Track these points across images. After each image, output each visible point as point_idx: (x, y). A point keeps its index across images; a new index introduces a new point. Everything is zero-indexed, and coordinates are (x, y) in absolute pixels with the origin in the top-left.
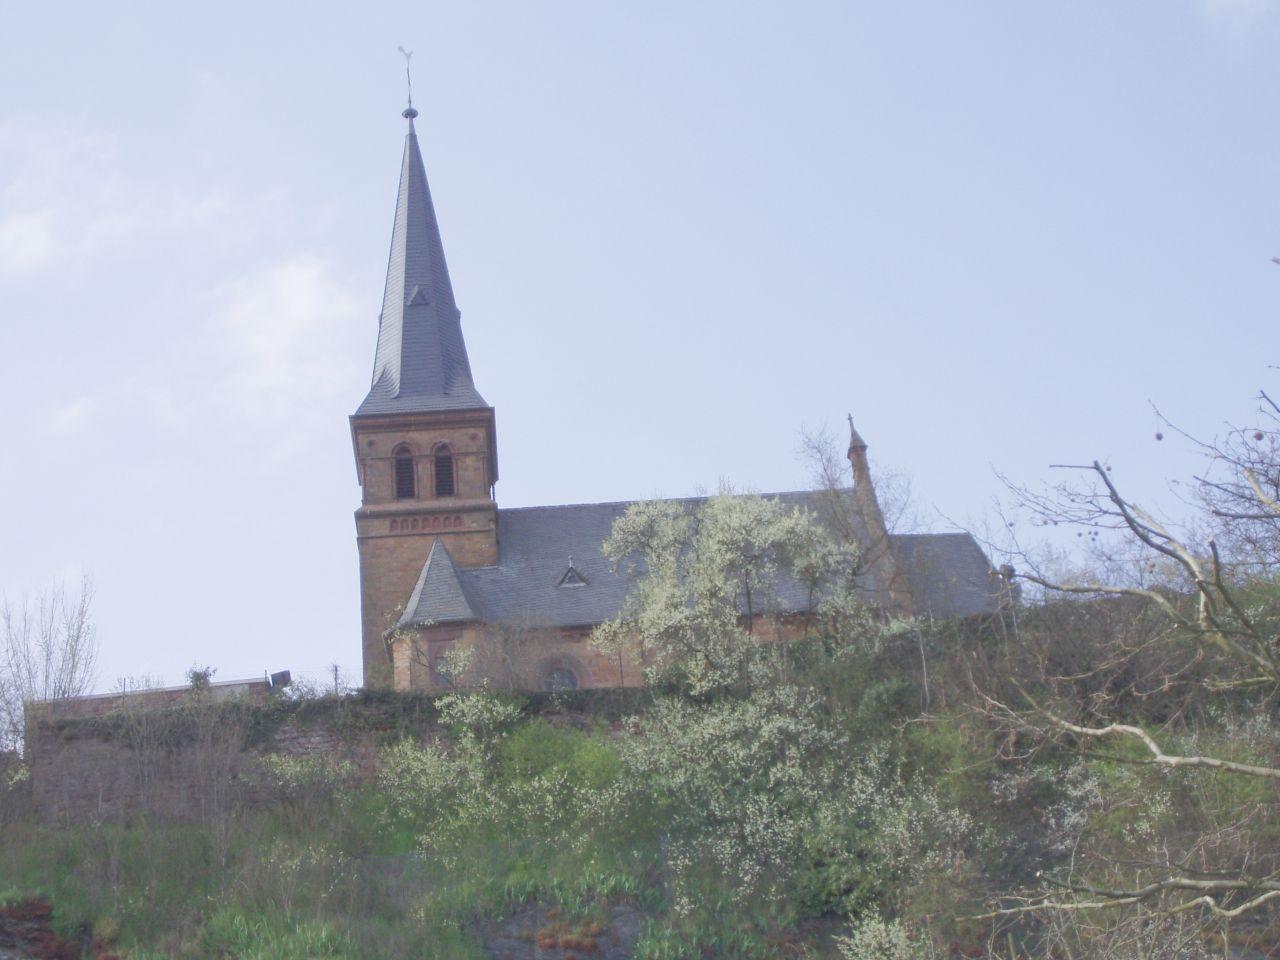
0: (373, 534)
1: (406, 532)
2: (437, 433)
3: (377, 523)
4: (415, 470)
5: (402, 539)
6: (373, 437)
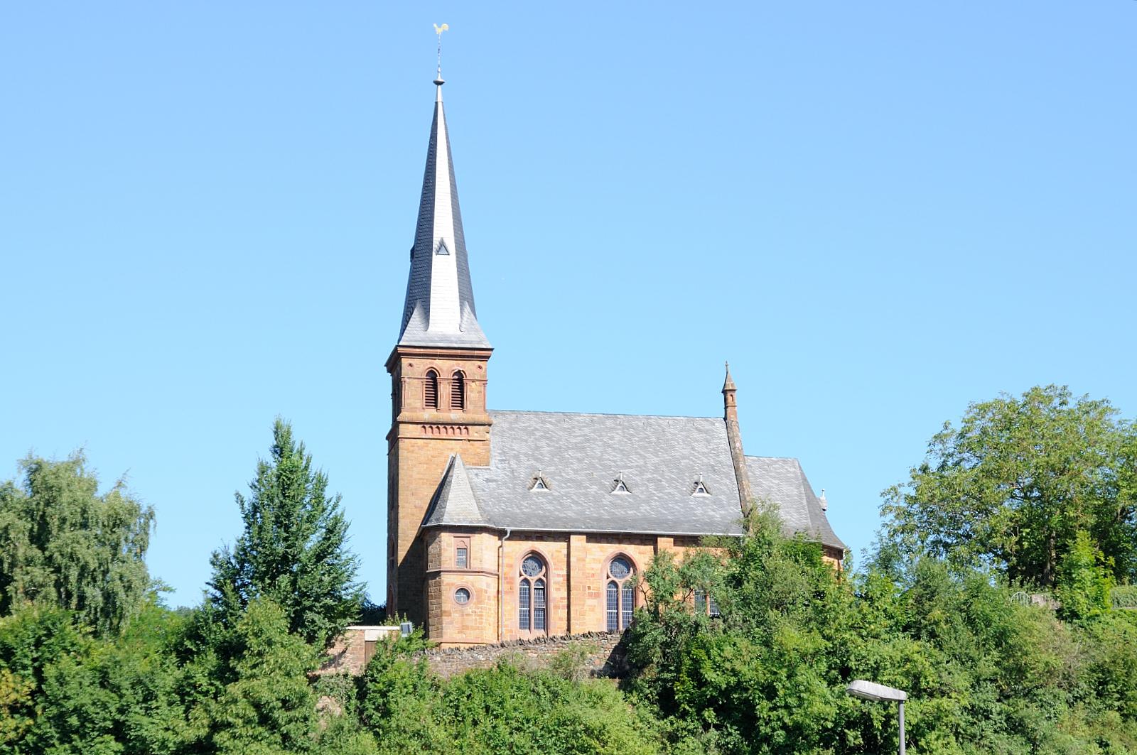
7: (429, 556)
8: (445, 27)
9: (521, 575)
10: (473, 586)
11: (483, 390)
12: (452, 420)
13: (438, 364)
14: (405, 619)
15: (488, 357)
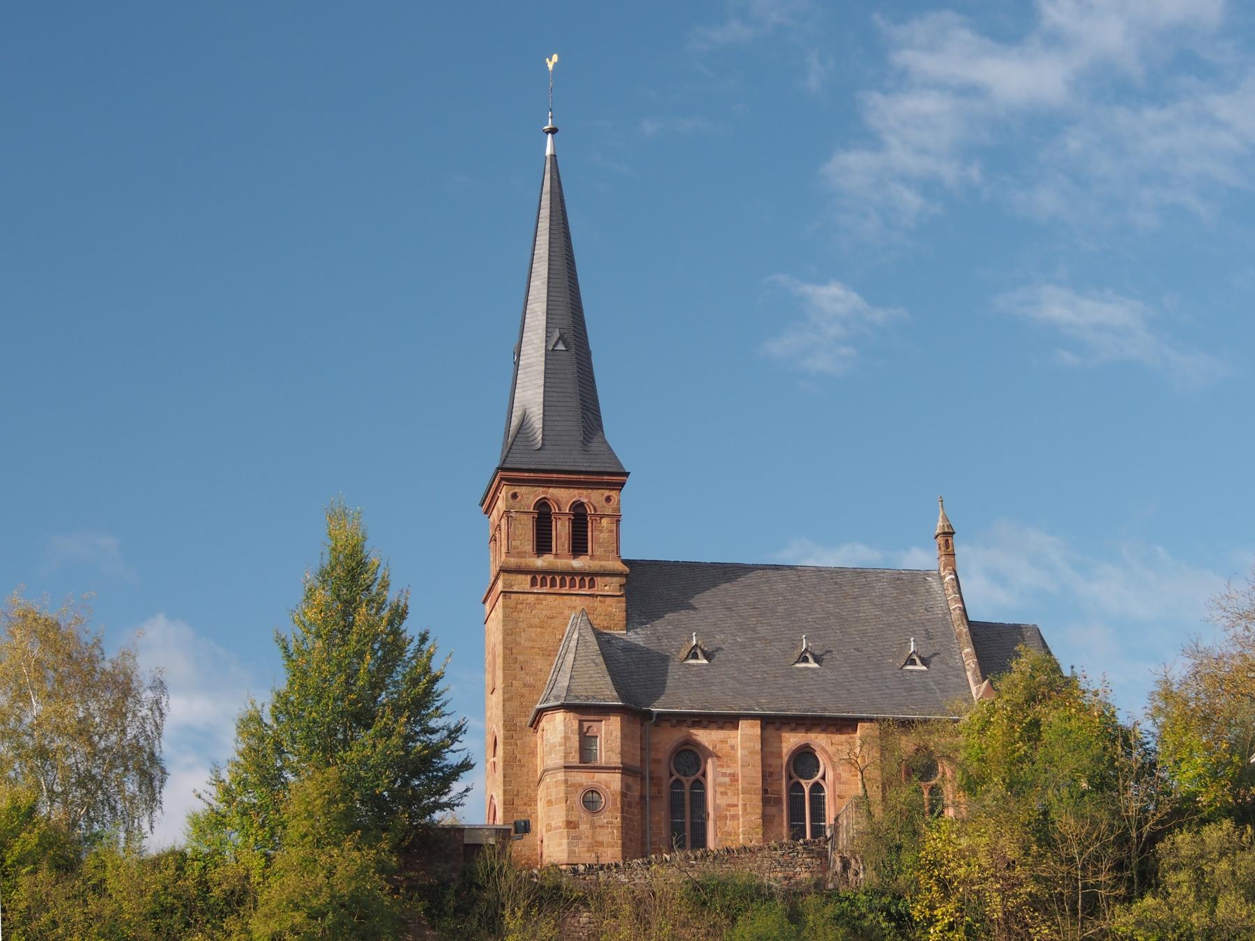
0: (515, 589)
1: (544, 590)
2: (576, 492)
3: (520, 577)
4: (499, 827)
5: (541, 596)
6: (517, 489)
7: (578, 739)
8: (555, 58)
9: (672, 775)
10: (608, 788)
11: (615, 528)
12: (573, 568)
13: (554, 493)
14: (822, 794)
15: (622, 484)
